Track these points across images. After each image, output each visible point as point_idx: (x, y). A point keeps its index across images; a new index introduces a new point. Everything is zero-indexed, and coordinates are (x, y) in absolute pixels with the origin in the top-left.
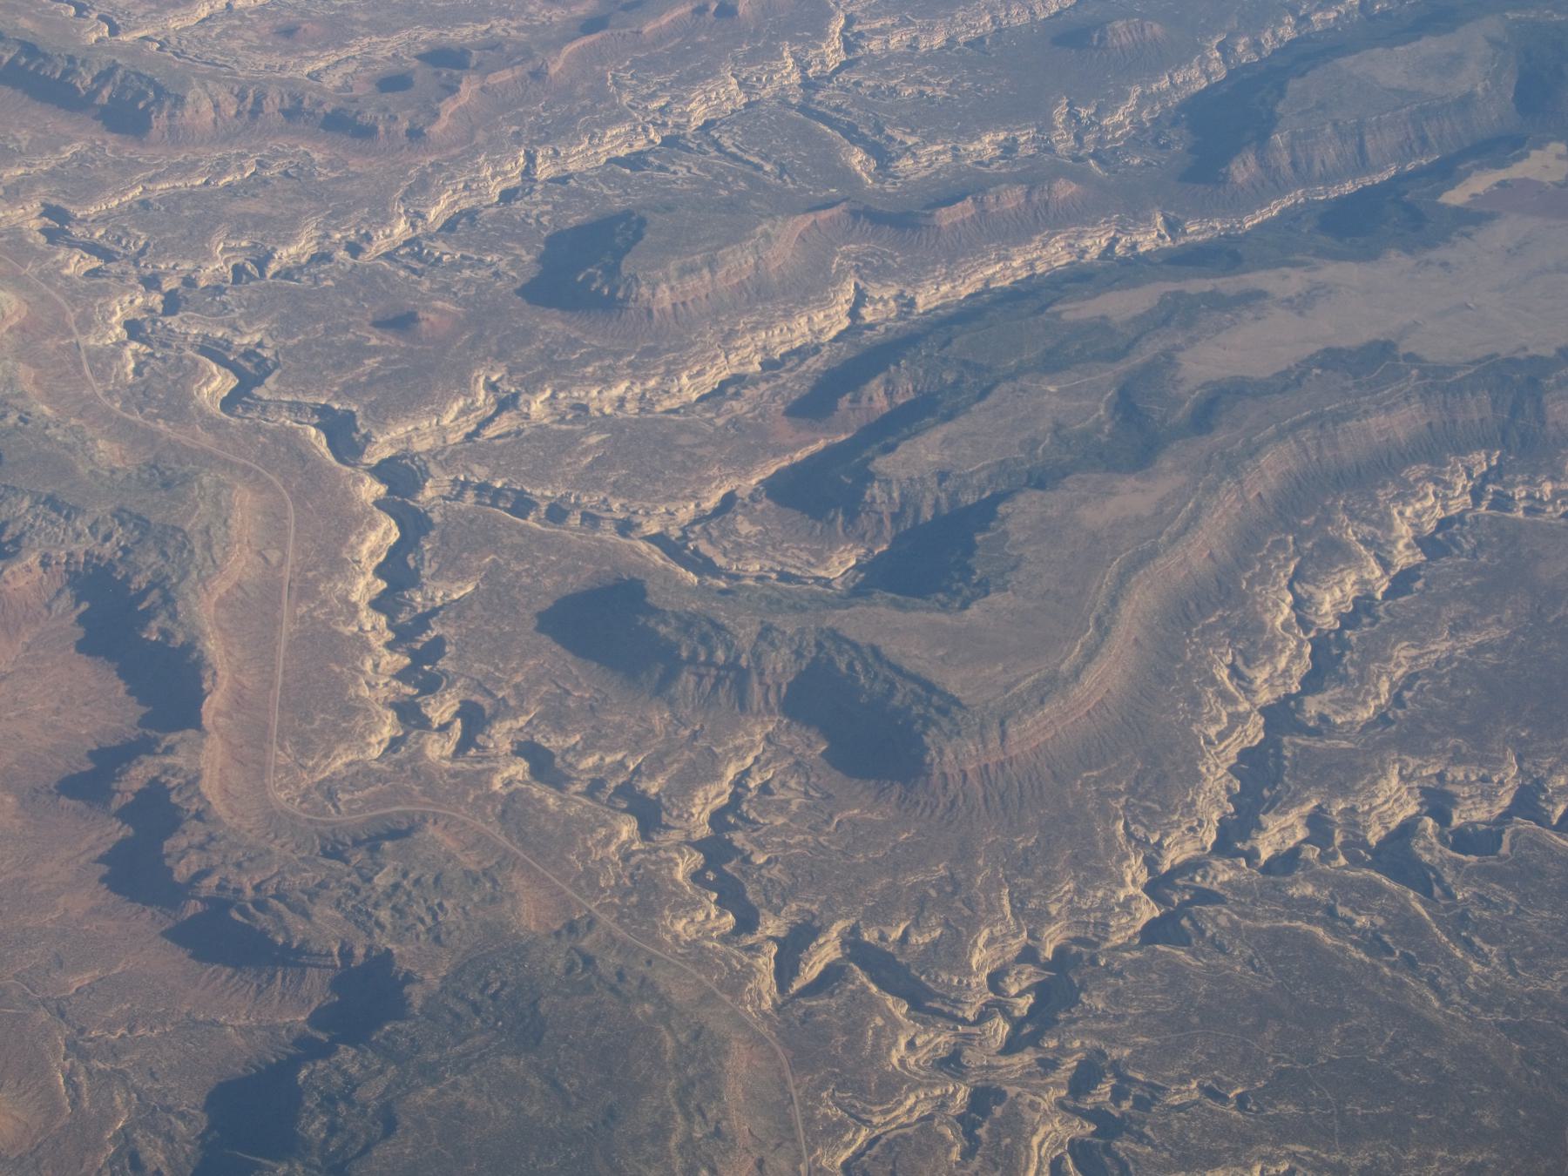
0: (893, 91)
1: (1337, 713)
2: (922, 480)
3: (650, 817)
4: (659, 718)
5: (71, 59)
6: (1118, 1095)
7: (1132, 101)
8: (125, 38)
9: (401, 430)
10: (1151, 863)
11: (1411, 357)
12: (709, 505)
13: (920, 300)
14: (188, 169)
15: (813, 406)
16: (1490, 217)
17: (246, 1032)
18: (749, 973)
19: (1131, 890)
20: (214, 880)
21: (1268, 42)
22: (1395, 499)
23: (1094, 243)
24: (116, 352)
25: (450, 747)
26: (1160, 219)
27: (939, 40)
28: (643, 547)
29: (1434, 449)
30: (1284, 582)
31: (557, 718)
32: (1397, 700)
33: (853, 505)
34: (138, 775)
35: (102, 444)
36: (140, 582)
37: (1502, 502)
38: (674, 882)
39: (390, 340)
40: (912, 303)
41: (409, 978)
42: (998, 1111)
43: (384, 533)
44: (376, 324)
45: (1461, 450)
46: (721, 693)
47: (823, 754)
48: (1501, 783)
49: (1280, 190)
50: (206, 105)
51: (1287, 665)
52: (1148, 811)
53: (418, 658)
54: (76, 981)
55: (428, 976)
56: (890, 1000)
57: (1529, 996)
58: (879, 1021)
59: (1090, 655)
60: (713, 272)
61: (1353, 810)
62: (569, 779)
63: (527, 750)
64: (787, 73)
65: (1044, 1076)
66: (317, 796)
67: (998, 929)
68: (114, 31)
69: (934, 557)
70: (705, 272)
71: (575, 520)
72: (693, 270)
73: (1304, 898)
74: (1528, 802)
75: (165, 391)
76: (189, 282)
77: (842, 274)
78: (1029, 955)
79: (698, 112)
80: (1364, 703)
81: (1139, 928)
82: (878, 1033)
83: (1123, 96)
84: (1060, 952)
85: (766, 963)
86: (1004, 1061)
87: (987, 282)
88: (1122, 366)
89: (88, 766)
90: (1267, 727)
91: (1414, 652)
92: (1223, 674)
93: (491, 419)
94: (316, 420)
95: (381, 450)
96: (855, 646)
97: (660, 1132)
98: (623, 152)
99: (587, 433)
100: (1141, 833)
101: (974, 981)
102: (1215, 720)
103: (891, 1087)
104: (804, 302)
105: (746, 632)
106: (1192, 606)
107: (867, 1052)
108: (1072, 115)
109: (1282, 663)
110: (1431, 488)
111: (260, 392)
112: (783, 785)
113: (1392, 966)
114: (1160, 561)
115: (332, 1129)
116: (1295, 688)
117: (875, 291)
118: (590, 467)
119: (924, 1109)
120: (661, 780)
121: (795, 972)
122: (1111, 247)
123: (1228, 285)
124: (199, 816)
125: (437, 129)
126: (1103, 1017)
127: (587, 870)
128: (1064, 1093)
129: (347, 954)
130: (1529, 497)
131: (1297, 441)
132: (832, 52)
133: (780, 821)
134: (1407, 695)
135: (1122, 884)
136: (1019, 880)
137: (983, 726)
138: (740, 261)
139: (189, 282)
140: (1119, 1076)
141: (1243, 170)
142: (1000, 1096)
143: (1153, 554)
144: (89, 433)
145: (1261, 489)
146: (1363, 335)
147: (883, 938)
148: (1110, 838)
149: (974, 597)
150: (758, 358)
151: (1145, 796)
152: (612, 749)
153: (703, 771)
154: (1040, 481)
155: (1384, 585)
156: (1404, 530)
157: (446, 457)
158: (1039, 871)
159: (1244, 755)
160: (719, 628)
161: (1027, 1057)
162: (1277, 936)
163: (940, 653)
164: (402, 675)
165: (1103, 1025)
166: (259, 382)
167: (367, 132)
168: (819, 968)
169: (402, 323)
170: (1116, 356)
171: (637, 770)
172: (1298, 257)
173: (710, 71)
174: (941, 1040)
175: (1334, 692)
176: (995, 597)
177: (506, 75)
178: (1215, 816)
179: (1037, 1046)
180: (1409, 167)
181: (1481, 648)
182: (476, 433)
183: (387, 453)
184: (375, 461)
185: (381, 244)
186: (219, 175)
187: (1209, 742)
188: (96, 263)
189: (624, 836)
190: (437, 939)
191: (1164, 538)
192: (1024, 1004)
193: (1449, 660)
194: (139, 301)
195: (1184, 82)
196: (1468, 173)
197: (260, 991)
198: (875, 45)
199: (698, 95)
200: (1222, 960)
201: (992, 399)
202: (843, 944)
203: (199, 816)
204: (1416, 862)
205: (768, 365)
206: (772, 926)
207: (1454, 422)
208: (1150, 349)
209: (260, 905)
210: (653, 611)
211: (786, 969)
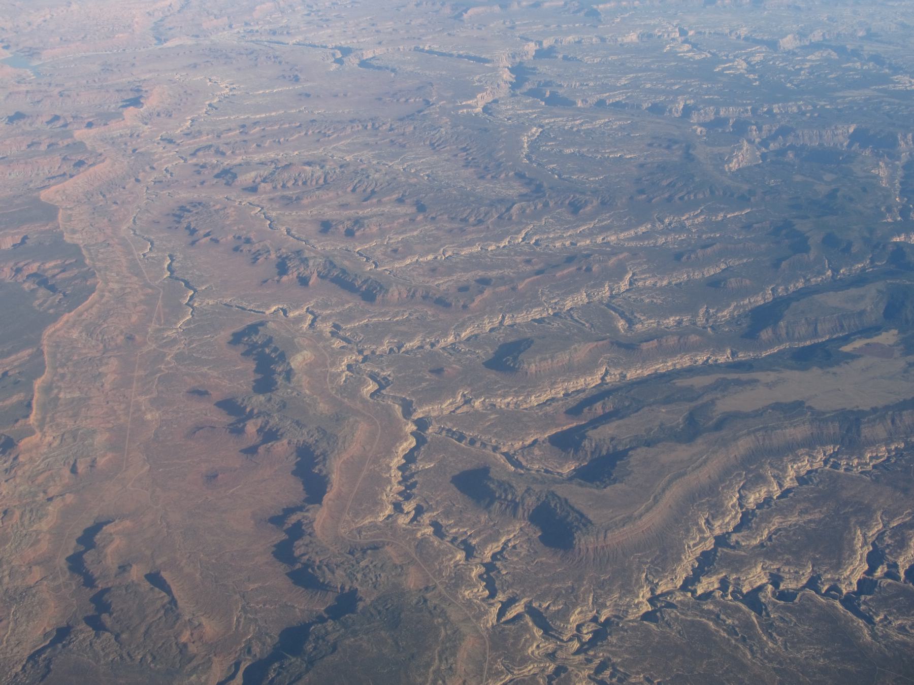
0: (642, 300)
3: (470, 551)
4: (484, 518)
5: (356, 275)
6: (612, 675)
7: (732, 307)
8: (379, 269)
10: (652, 590)
11: (810, 408)
12: (527, 443)
13: (628, 375)
15: (575, 412)
16: (860, 356)
17: (302, 611)
18: (486, 613)
19: (641, 599)
20: (307, 557)
21: (791, 288)
22: (791, 461)
23: (701, 359)
24: (340, 375)
25: (408, 520)
26: (729, 351)
27: (665, 283)
28: (498, 456)
29: (811, 444)
30: (737, 489)
31: (447, 514)
32: (770, 539)
33: (577, 447)
34: (294, 518)
35: (321, 405)
36: (318, 452)
37: (836, 466)
38: (470, 577)
39: (434, 377)
40: (625, 376)
41: (361, 599)
42: (563, 675)
43: (412, 442)
44: (432, 371)
45: (823, 444)
46: (508, 510)
47: (540, 537)
48: (803, 574)
49: (780, 342)
50: (396, 293)
51: (731, 519)
52: (657, 571)
53: (407, 487)
54: (252, 586)
55: (367, 599)
56: (535, 629)
57: (790, 659)
58: (528, 636)
60: (552, 361)
61: (739, 578)
62: (446, 536)
63: (435, 525)
64: (606, 292)
65: (586, 665)
66: (355, 532)
67: (585, 608)
68: (376, 266)
69: (601, 469)
70: (550, 361)
71: (478, 444)
72: (545, 359)
73: (708, 610)
74: (813, 583)
75: (351, 390)
76: (373, 353)
77: (602, 364)
78: (595, 619)
79: (569, 304)
80: (755, 538)
81: (641, 614)
82: (526, 640)
83: (729, 306)
84: (607, 620)
85: (495, 610)
86: (572, 657)
87: (657, 370)
88: (693, 404)
89: (281, 514)
90: (715, 544)
91: (781, 520)
92: (702, 522)
93: (459, 407)
95: (419, 414)
96: (559, 498)
97: (428, 665)
98: (538, 317)
99: (491, 414)
100: (651, 578)
101: (569, 626)
102: (694, 539)
103: (525, 660)
105: (520, 490)
107: (519, 648)
108: (707, 312)
109: (727, 520)
110: (807, 458)
111: (384, 392)
112: (521, 546)
113: (736, 640)
115: (315, 648)
116: (731, 529)
117: (612, 371)
118: (489, 426)
119: (536, 671)
120: (477, 540)
121: (504, 615)
122: (707, 360)
123: (744, 376)
124: (310, 535)
125: (473, 305)
126: (614, 646)
127: (440, 569)
128: (592, 672)
129: (342, 588)
130: (847, 464)
132: (624, 285)
133: (516, 559)
134: (774, 536)
135: (638, 597)
136: (598, 591)
138: (563, 357)
139: (373, 353)
140: (614, 669)
141: (766, 334)
142: (566, 670)
143: (685, 474)
144: (319, 400)
146: (793, 398)
147: (540, 606)
148: (638, 580)
149: (610, 484)
150: (563, 392)
151: (657, 565)
152: (463, 527)
153: (494, 538)
154: (648, 444)
155: (779, 493)
156: (791, 473)
157: (439, 419)
158: (606, 588)
159: (703, 553)
160: (511, 487)
161: (581, 657)
162: (693, 623)
163: (590, 503)
164: (400, 493)
165: (614, 649)
166: (384, 388)
168: (514, 614)
169: (438, 371)
170: (692, 400)
171: (470, 535)
172: (776, 368)
173: (577, 290)
174: (551, 646)
175: (745, 533)
176: (618, 486)
177: (503, 288)
178: (684, 576)
179: (586, 654)
180: (834, 337)
181: (810, 521)
182: (454, 412)
183: (421, 416)
185: (442, 343)
186: (395, 317)
187: (689, 547)
188: (345, 344)
189: (458, 558)
190: (375, 587)
191: (690, 468)
192: (587, 637)
193: (795, 525)
194: (354, 358)
196: (855, 340)
197: (311, 597)
198: (640, 284)
199: (570, 298)
200: (668, 630)
201: (639, 413)
202: (525, 607)
203: (310, 535)
204: (759, 600)
205: (566, 395)
206: (501, 597)
209: (319, 567)
210: (490, 479)
211: (501, 613)
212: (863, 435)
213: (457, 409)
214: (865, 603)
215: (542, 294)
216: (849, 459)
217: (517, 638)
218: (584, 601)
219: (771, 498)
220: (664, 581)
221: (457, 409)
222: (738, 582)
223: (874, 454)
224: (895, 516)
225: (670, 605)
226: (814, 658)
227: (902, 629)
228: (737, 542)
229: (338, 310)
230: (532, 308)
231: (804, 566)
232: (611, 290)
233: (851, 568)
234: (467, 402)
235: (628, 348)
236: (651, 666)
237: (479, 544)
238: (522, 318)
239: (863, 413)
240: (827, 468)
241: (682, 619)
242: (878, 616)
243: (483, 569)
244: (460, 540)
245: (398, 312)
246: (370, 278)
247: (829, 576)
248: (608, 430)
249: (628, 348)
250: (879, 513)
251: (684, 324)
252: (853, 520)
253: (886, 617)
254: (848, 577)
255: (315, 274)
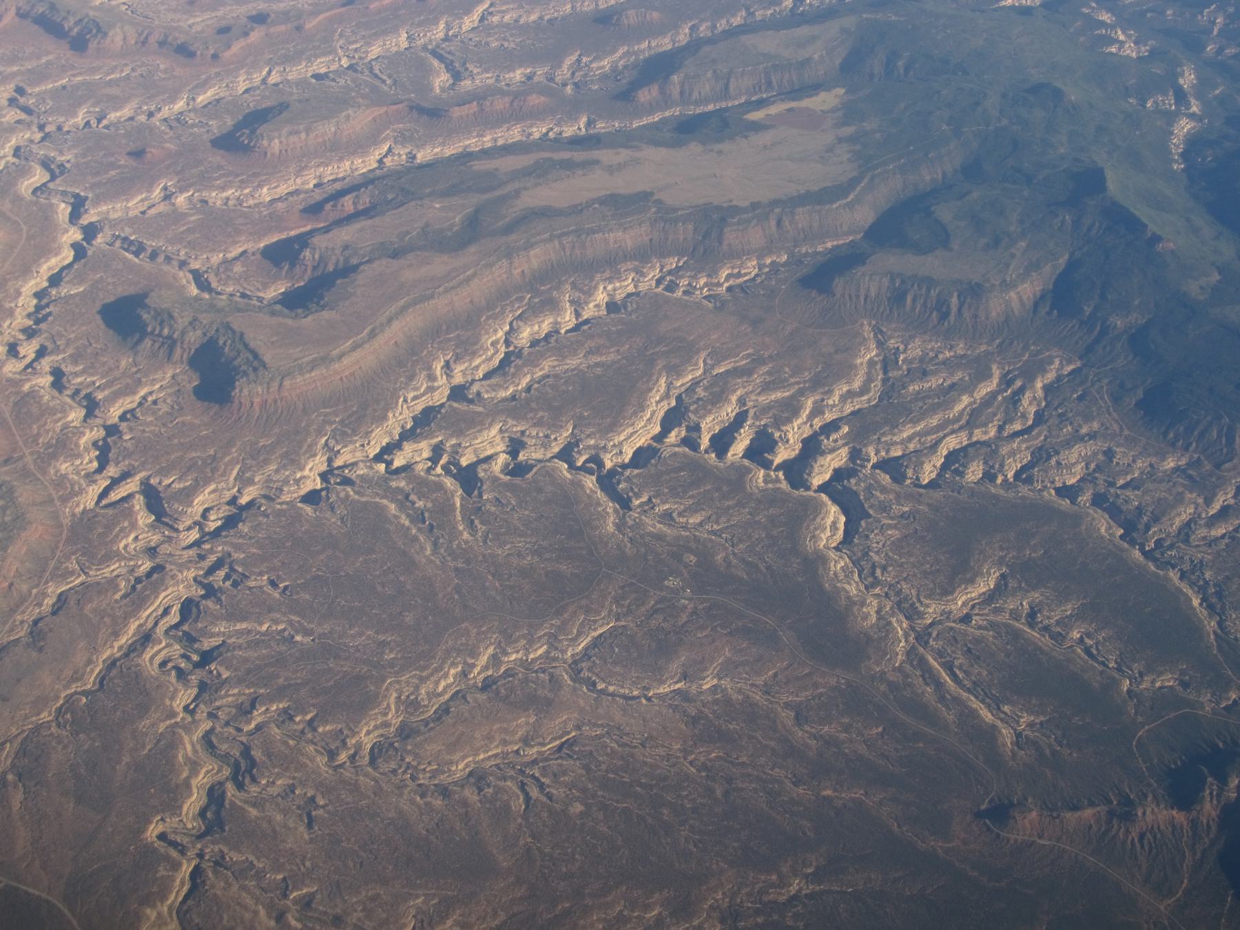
0: (487, 43)
1: (487, 392)
2: (333, 249)
3: (92, 406)
5: (68, 12)
6: (227, 577)
7: (618, 55)
9: (105, 208)
10: (330, 461)
11: (659, 202)
12: (230, 256)
13: (419, 156)
14: (94, 71)
15: (314, 210)
18: (81, 491)
19: (306, 472)
21: (722, 25)
23: (537, 132)
25: (20, 366)
26: (584, 120)
27: (533, 17)
29: (642, 256)
30: (509, 319)
32: (528, 389)
37: (671, 287)
39: (132, 162)
40: (414, 157)
44: (129, 154)
48: (556, 439)
49: (667, 106)
50: (119, 39)
51: (481, 364)
59: (355, 347)
61: (460, 445)
62: (65, 388)
64: (439, 31)
65: (197, 563)
67: (223, 485)
70: (303, 135)
71: (161, 259)
72: (297, 132)
73: (397, 488)
74: (566, 454)
76: (59, 128)
77: (386, 139)
78: (233, 501)
81: (302, 493)
84: (251, 504)
85: (94, 491)
87: (466, 147)
91: (556, 363)
94: (72, 200)
96: (234, 332)
98: (323, 71)
100: (332, 443)
104: (354, 153)
106: (444, 327)
108: (579, 61)
109: (477, 362)
112: (164, 401)
113: (419, 530)
114: (432, 302)
122: (547, 133)
123: (579, 156)
125: (227, 54)
130: (689, 284)
131: (560, 243)
133: (150, 419)
134: (536, 386)
137: (271, 379)
138: (327, 129)
139: (59, 128)
141: (646, 95)
143: (431, 297)
145: (525, 267)
150: (315, 182)
151: (347, 426)
152: (93, 375)
153: (129, 390)
156: (601, 297)
157: (114, 224)
160: (171, 317)
161: (192, 552)
163: (275, 339)
165: (240, 541)
167: (191, 55)
169: (138, 154)
173: (395, 30)
174: (155, 538)
176: (326, 314)
177: (282, 28)
181: (597, 365)
183: (94, 219)
184: (86, 223)
185: (165, 112)
186: (108, 74)
187: (405, 401)
188: (23, 116)
189: (70, 418)
191: (441, 289)
192: (212, 526)
193: (573, 370)
195: (657, 46)
202: (142, 483)
206: (112, 471)
207: (667, 239)
208: (509, 188)
212: (725, 243)
213: (149, 208)
214: (628, 479)
215: (341, 35)
216: (694, 277)
217: (108, 528)
218: (223, 475)
219: (557, 332)
220: (350, 447)
221: (149, 208)
222: (456, 451)
223: (736, 271)
224: (725, 358)
225: (347, 481)
226: (519, 555)
227: (667, 517)
228: (478, 394)
229: (28, 66)
230: (316, 57)
231: (559, 427)
232: (448, 27)
233: (630, 430)
234: (167, 197)
235: (431, 115)
236: (283, 563)
237: (105, 399)
238: (296, 72)
239: (735, 210)
240: (660, 290)
241: (353, 501)
242: (638, 496)
243: (102, 433)
244: (83, 393)
245: (115, 67)
246: (87, 15)
247: (592, 442)
248: (345, 234)
249: (431, 115)
250: (703, 355)
251: (536, 79)
252: (660, 364)
253: (650, 500)
254: (621, 443)
255: (13, 11)
